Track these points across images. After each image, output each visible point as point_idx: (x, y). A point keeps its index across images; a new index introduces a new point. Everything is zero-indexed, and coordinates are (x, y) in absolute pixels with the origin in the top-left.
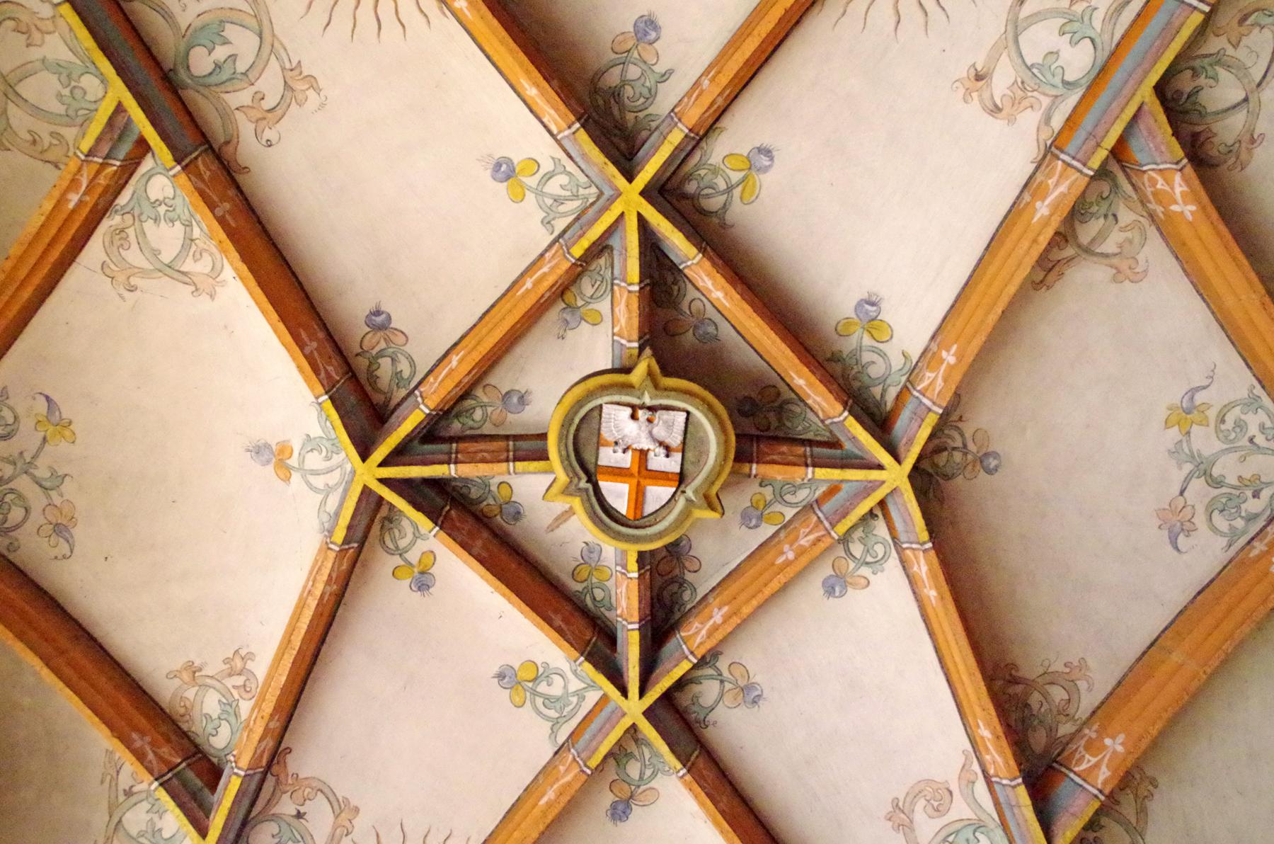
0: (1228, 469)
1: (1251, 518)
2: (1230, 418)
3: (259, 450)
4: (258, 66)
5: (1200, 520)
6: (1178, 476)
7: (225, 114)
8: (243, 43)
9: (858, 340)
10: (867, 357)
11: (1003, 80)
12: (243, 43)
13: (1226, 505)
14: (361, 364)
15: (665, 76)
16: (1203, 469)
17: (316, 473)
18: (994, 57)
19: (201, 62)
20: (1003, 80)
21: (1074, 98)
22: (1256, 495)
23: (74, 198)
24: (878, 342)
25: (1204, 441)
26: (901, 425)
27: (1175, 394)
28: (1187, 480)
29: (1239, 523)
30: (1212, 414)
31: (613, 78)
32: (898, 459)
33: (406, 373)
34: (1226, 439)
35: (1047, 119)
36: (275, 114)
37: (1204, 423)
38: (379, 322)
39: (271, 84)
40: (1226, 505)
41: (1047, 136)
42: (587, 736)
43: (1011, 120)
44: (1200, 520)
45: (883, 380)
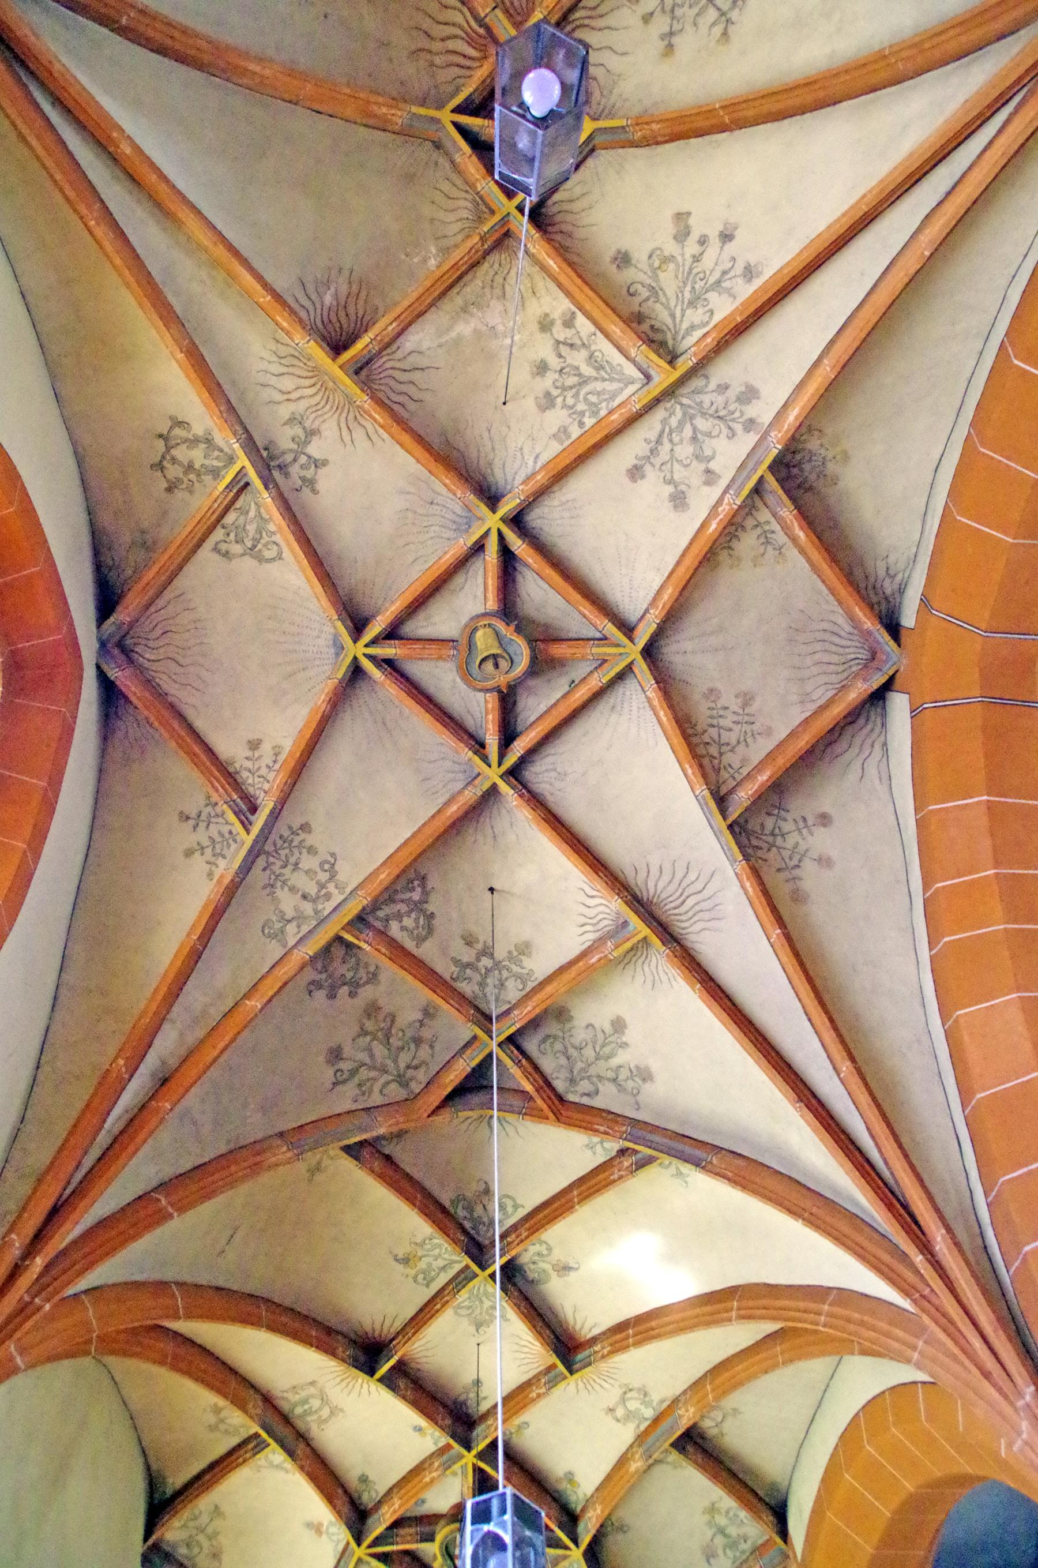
0: (733, 1531)
1: (743, 1552)
2: (731, 1514)
3: (309, 1525)
4: (320, 1409)
5: (720, 1552)
6: (710, 1533)
7: (307, 1423)
8: (316, 1403)
9: (564, 1486)
10: (569, 1492)
11: (620, 1412)
12: (316, 1403)
13: (733, 1545)
14: (355, 1495)
15: (485, 1398)
16: (722, 1531)
17: (333, 1534)
18: (617, 1404)
19: (298, 1410)
20: (620, 1412)
21: (647, 1423)
22: (745, 1541)
23: (383, 950)
24: (700, 892)
25: (722, 1521)
26: (581, 1528)
27: (706, 1503)
28: (714, 1535)
29: (738, 1554)
30: (723, 1511)
31: (462, 1398)
32: (577, 1546)
33: (374, 1496)
34: (730, 1519)
35: (638, 1426)
36: (326, 1421)
37: (720, 1513)
38: (364, 1479)
39: (325, 1412)
40: (733, 1545)
41: (638, 1432)
42: (541, 1215)
43: (624, 1424)
44: (720, 1552)
45: (576, 1503)
